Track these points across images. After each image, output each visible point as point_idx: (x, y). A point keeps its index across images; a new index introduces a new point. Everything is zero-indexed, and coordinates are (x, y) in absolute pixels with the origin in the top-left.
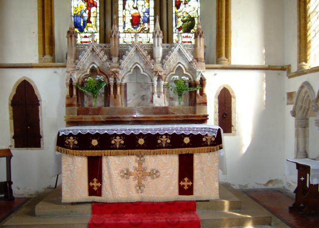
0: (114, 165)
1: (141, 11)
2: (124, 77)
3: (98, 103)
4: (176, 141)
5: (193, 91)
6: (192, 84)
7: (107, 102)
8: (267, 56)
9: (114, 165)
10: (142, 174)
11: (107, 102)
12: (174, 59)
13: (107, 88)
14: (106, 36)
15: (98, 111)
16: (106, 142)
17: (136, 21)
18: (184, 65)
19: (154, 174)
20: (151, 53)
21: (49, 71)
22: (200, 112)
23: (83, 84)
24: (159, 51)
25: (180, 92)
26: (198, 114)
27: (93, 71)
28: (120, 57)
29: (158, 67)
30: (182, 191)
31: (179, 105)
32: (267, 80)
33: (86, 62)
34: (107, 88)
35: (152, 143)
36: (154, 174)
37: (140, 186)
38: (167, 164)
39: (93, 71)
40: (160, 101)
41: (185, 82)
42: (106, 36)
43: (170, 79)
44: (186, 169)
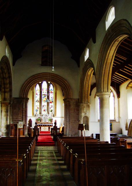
0: (42, 128)
1: (45, 109)
2: (43, 118)
3: (39, 121)
4: (48, 125)
5: (51, 120)
6: (51, 119)
7: (40, 121)
8: (61, 116)
9: (42, 128)
10: (45, 129)
11: (40, 121)
12: (49, 116)
13: (41, 120)
14: (40, 113)
15: (39, 123)
16: (41, 125)
17: (44, 110)
18: (50, 117)
19: (46, 129)
20: (46, 115)
21: (33, 118)
22: (52, 123)
23: (38, 119)
24: (47, 115)
25: (50, 120)
26: (101, 140)
27: (39, 118)
28: (42, 116)
29: (47, 117)
30: (49, 130)
31: (50, 122)
32: (61, 119)
33: (38, 116)
34: (41, 120)
35: (46, 126)
36: (46, 129)
37: (45, 130)
38: (47, 128)
39: (39, 118)
40: (47, 121)
41: (84, 103)
42: (40, 113)
43: (131, 26)
44: (49, 128)
